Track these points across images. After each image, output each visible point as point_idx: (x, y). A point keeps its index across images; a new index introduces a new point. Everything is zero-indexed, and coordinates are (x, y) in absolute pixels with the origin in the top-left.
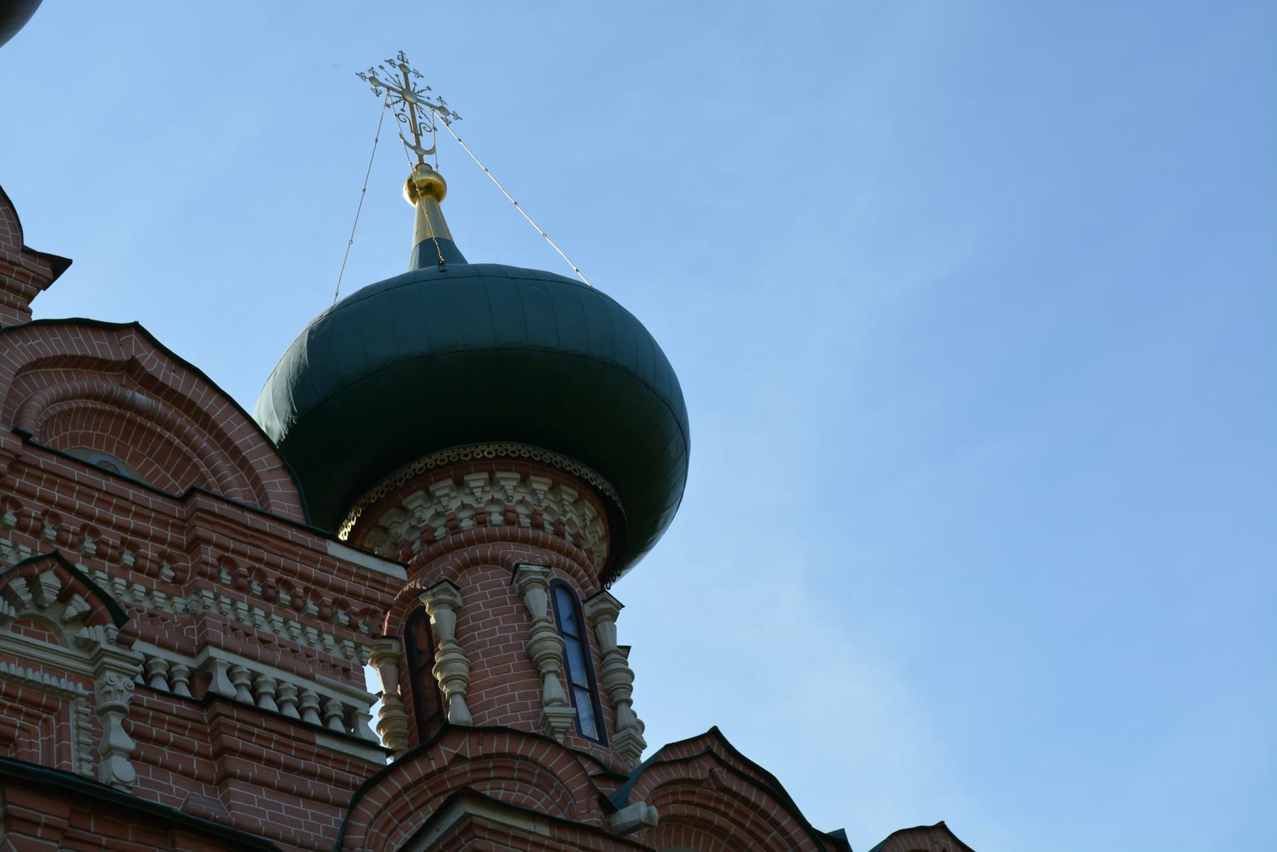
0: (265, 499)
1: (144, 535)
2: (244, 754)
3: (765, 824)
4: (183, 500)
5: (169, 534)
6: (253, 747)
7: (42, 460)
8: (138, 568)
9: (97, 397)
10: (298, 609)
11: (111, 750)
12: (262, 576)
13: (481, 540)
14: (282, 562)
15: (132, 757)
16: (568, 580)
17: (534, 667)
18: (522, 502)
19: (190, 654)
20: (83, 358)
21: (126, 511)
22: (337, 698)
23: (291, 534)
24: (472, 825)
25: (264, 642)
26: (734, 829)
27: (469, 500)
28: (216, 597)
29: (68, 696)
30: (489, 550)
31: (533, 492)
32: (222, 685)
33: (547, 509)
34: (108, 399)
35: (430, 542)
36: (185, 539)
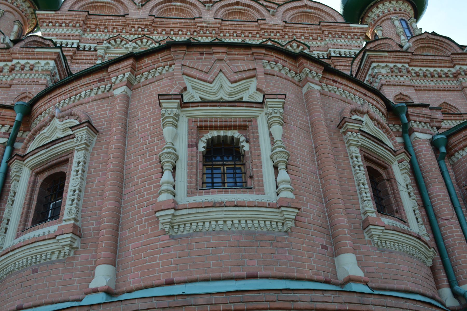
0: (336, 20)
1: (313, 33)
2: (340, 65)
3: (442, 43)
4: (319, 25)
5: (318, 32)
6: (341, 64)
7: (290, 25)
8: (313, 39)
9: (300, 13)
10: (347, 38)
12: (338, 34)
13: (384, 16)
14: (341, 30)
16: (404, 18)
18: (391, 7)
19: (327, 51)
20: (296, 7)
21: (308, 30)
23: (342, 25)
24: (369, 57)
25: (341, 45)
26: (436, 46)
27: (380, 10)
28: (329, 40)
30: (385, 18)
31: (393, 4)
32: (333, 54)
33: (397, 7)
34: (302, 12)
35: (375, 21)
36: (321, 32)
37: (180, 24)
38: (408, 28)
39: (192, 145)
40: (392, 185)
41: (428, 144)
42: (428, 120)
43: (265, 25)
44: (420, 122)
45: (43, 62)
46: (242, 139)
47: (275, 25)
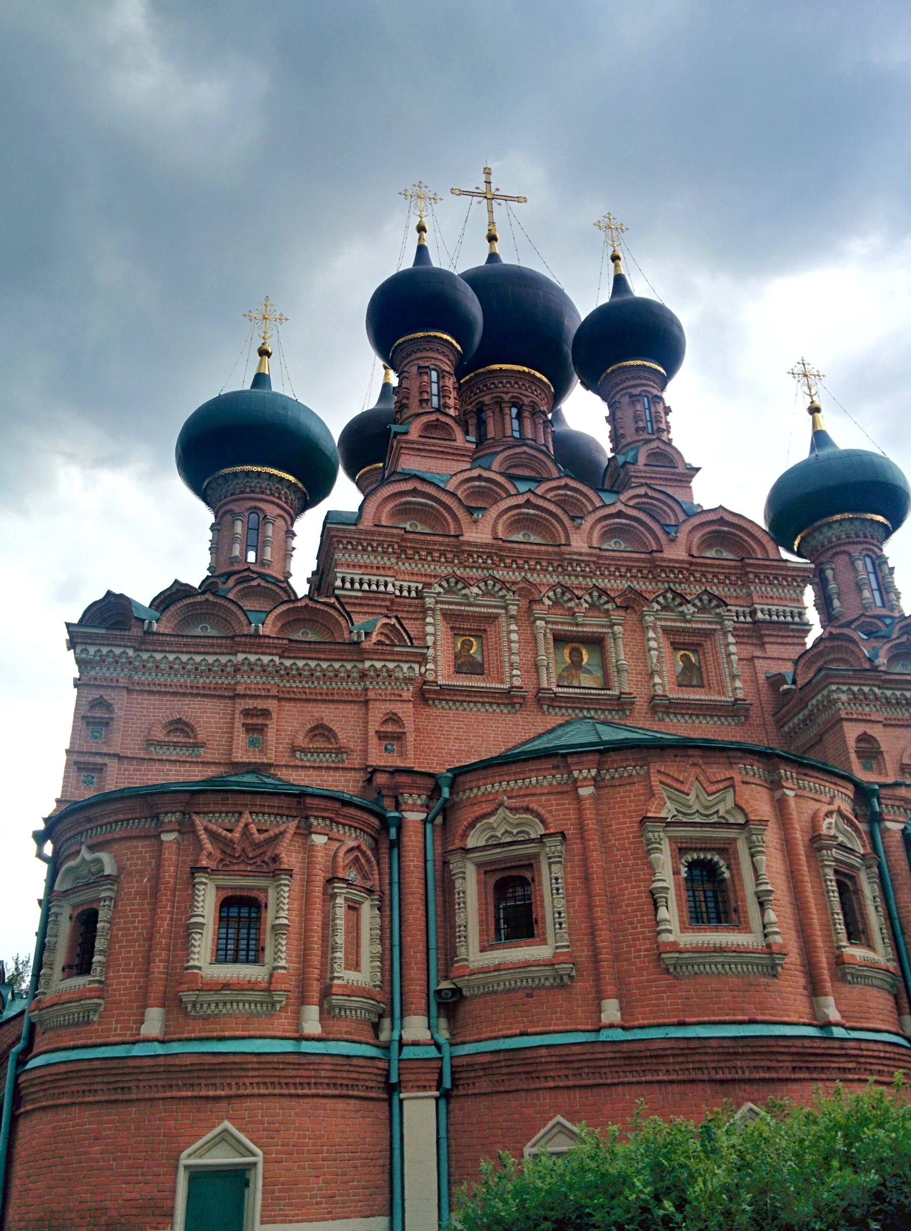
7: (698, 560)
11: (728, 644)
15: (736, 643)
17: (859, 588)
22: (796, 610)
29: (715, 630)
37: (539, 552)
38: (875, 573)
39: (676, 872)
40: (858, 899)
41: (899, 835)
42: (902, 803)
43: (663, 560)
44: (892, 806)
45: (405, 666)
46: (722, 863)
47: (677, 561)
